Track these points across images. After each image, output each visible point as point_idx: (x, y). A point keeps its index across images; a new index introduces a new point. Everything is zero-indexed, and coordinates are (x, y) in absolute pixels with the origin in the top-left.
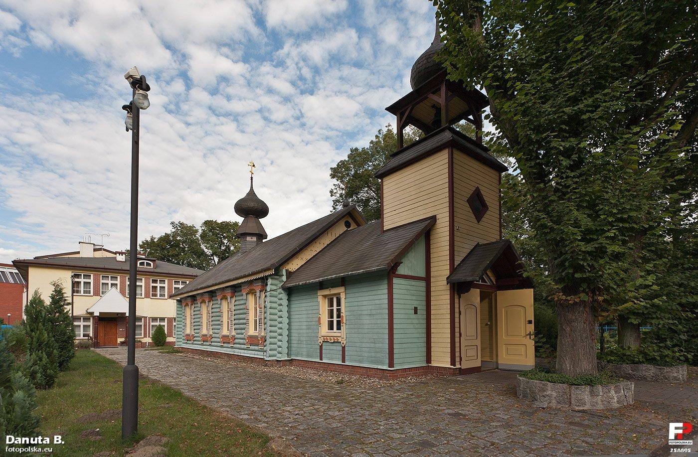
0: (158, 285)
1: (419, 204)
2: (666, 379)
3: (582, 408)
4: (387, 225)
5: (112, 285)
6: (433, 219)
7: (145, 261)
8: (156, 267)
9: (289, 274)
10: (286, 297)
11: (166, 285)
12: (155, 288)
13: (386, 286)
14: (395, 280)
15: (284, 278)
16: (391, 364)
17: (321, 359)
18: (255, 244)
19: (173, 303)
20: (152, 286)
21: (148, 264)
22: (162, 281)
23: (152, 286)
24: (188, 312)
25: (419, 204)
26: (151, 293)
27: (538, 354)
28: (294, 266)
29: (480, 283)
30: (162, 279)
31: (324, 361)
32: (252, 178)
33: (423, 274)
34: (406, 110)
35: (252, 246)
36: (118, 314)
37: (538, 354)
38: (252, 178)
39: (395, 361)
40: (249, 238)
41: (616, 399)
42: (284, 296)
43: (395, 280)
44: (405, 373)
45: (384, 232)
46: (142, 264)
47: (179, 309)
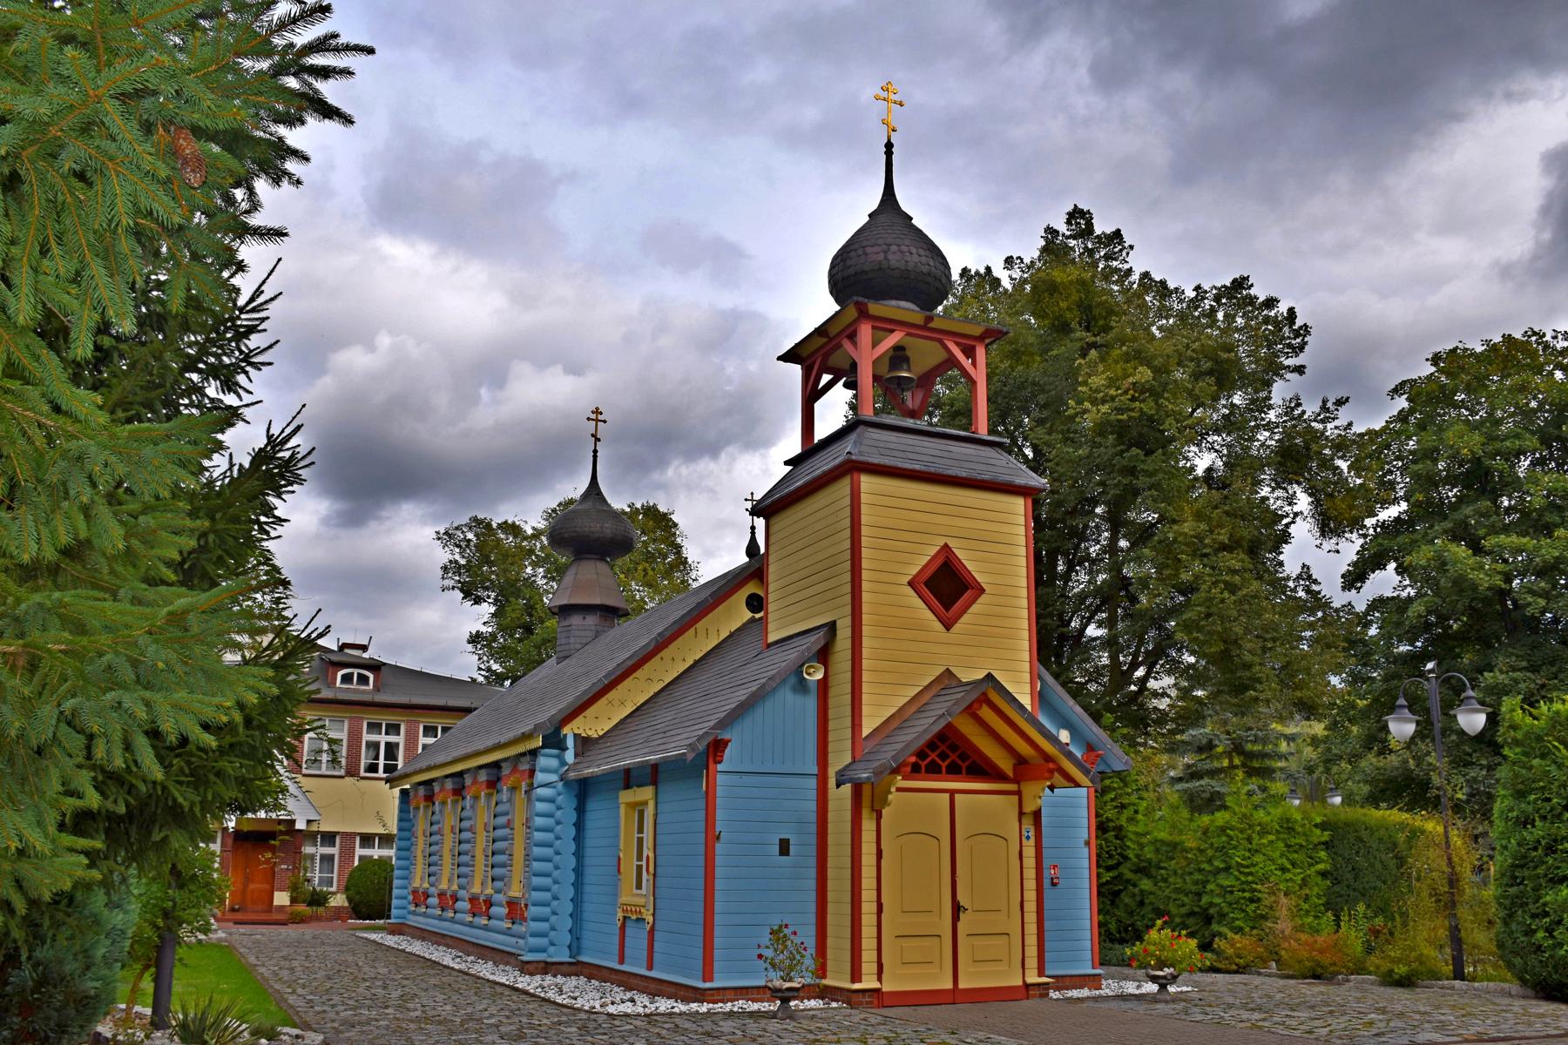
1: (811, 591)
3: (664, 1005)
5: (323, 857)
6: (832, 627)
7: (356, 671)
8: (377, 688)
9: (584, 743)
10: (574, 803)
11: (400, 739)
15: (570, 756)
17: (622, 961)
20: (398, 734)
21: (363, 680)
22: (393, 729)
23: (398, 734)
25: (811, 591)
27: (404, 815)
28: (593, 724)
30: (392, 718)
32: (889, 146)
34: (814, 362)
35: (584, 641)
37: (404, 815)
38: (889, 146)
45: (769, 646)
46: (347, 679)
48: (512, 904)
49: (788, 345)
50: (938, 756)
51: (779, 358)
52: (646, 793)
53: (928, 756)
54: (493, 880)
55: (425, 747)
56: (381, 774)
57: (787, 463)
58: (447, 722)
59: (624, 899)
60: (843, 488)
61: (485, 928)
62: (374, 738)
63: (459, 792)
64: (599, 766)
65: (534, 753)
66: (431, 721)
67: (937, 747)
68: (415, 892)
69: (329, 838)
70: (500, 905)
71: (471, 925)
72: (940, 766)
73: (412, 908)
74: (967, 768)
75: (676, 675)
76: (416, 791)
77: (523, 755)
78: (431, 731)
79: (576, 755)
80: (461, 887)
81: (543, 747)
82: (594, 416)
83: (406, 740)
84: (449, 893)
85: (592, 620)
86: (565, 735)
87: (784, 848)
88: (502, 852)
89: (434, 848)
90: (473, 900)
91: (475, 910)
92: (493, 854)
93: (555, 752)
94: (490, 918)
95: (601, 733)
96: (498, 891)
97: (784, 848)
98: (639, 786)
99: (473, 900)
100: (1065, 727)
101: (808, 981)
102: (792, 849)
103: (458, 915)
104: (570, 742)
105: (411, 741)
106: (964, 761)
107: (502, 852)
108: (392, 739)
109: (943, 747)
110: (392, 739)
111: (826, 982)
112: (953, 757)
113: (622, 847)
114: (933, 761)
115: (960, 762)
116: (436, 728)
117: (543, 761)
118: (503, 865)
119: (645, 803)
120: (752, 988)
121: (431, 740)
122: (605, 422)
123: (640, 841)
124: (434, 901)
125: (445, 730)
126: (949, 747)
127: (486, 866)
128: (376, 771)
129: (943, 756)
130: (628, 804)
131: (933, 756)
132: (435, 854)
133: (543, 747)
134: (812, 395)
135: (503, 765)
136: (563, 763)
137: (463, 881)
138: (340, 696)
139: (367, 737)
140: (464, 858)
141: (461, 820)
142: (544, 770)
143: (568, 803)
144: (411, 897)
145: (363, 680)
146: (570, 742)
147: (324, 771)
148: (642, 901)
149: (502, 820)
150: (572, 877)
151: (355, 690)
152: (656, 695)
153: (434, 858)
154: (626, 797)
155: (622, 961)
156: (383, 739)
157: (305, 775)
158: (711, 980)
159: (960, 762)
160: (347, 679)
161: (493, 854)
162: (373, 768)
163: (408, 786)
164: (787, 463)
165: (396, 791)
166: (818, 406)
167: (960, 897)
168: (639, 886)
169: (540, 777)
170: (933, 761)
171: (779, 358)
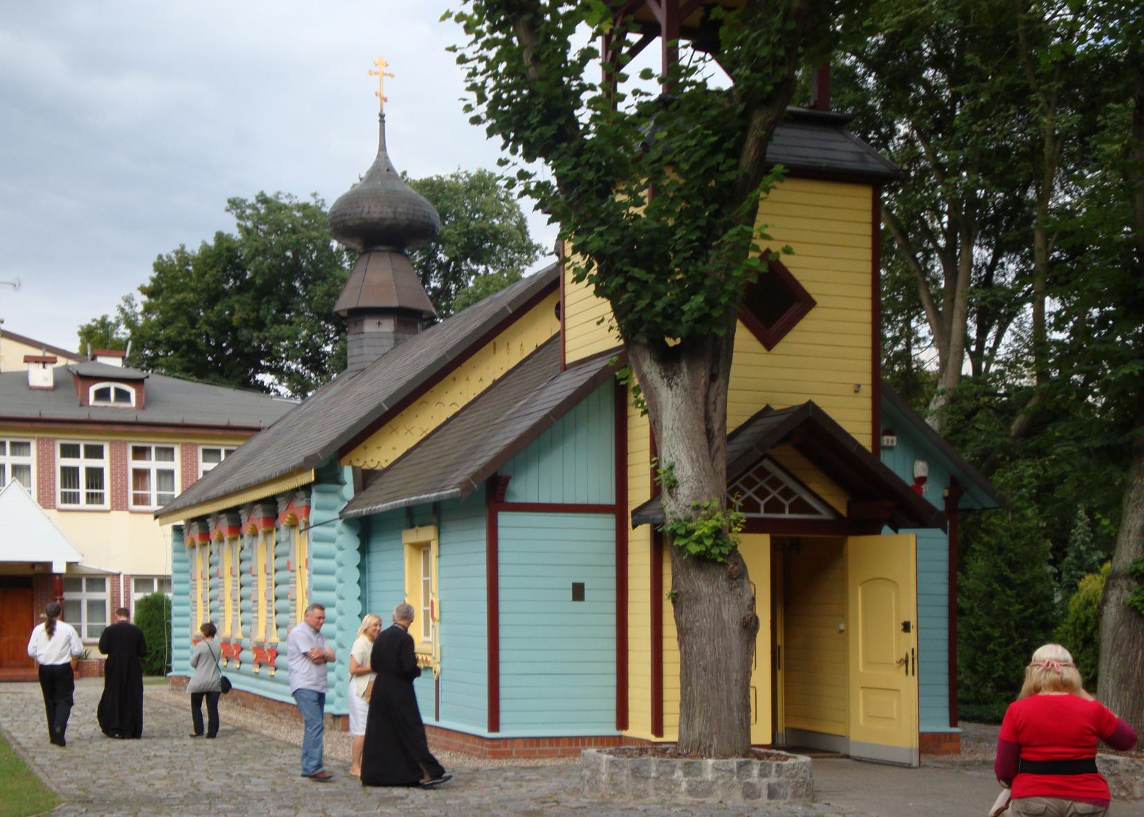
0: (153, 465)
2: (1124, 788)
4: (570, 358)
5: (16, 469)
7: (113, 386)
8: (144, 403)
9: (366, 479)
10: (356, 543)
11: (176, 465)
12: (141, 475)
13: (483, 534)
14: (504, 518)
15: (348, 491)
16: (494, 724)
17: (437, 719)
18: (389, 343)
19: (163, 533)
20: (172, 459)
21: (122, 396)
22: (166, 453)
24: (200, 564)
26: (131, 492)
29: (787, 515)
30: (165, 443)
31: (502, 733)
32: (382, 116)
33: (609, 498)
35: (382, 351)
36: (33, 565)
38: (382, 116)
39: (504, 717)
40: (370, 326)
41: (684, 786)
42: (348, 542)
43: (504, 518)
44: (538, 749)
46: (102, 395)
47: (180, 556)
50: (755, 493)
53: (768, 494)
54: (277, 627)
55: (205, 473)
58: (232, 444)
61: (272, 679)
62: (70, 462)
63: (236, 529)
64: (377, 503)
65: (307, 488)
66: (212, 444)
69: (96, 581)
71: (257, 675)
74: (766, 505)
75: (471, 397)
77: (296, 490)
78: (210, 454)
80: (245, 635)
82: (376, 69)
83: (112, 464)
85: (388, 326)
87: (578, 592)
88: (285, 597)
89: (214, 592)
91: (262, 660)
94: (276, 669)
95: (385, 465)
96: (284, 639)
97: (578, 592)
98: (421, 525)
100: (922, 458)
101: (785, 763)
103: (243, 666)
105: (189, 466)
106: (787, 499)
107: (285, 597)
108: (94, 463)
109: (762, 483)
110: (94, 463)
111: (624, 733)
112: (774, 494)
113: (407, 591)
115: (783, 500)
116: (78, 447)
118: (287, 611)
120: (544, 738)
121: (210, 466)
122: (392, 76)
123: (427, 584)
124: (248, 655)
125: (228, 452)
126: (768, 483)
127: (269, 612)
129: (762, 493)
137: (246, 628)
139: (62, 462)
140: (246, 603)
145: (122, 396)
149: (282, 562)
152: (448, 421)
153: (214, 604)
155: (437, 719)
156: (82, 463)
157: (133, 512)
160: (102, 395)
163: (181, 523)
165: (168, 529)
169: (315, 515)
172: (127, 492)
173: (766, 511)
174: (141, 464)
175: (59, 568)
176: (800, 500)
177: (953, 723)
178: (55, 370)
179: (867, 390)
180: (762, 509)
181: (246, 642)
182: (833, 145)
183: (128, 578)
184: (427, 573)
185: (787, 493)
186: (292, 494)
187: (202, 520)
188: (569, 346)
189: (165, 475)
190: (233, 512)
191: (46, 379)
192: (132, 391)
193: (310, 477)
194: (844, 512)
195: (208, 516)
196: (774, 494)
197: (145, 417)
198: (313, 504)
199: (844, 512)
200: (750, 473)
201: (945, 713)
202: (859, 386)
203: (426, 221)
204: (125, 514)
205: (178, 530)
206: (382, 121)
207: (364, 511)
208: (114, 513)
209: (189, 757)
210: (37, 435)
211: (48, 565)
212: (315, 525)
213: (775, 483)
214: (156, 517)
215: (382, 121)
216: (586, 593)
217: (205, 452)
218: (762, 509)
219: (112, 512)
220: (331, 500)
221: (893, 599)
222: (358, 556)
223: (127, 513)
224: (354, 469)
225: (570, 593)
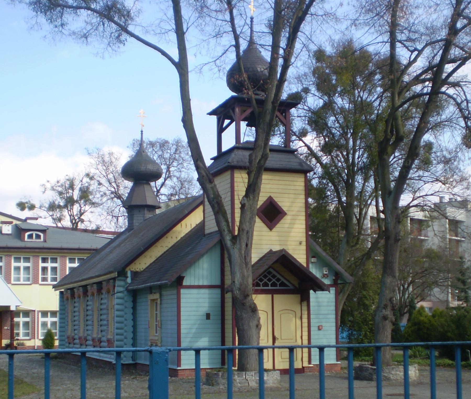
0: (49, 265)
7: (34, 233)
8: (45, 241)
9: (135, 274)
10: (131, 299)
15: (129, 280)
21: (38, 237)
22: (54, 260)
30: (54, 256)
32: (142, 132)
38: (142, 132)
43: (183, 291)
48: (108, 341)
49: (210, 110)
50: (276, 280)
51: (208, 114)
52: (157, 296)
53: (263, 280)
54: (101, 331)
56: (49, 282)
57: (212, 159)
59: (151, 338)
60: (227, 176)
65: (114, 279)
67: (267, 277)
68: (68, 337)
69: (27, 313)
70: (104, 342)
72: (277, 284)
73: (67, 345)
76: (67, 292)
79: (132, 279)
81: (118, 277)
84: (83, 338)
86: (127, 272)
90: (93, 340)
92: (101, 320)
93: (123, 278)
99: (93, 340)
102: (211, 317)
104: (129, 274)
108: (54, 265)
109: (270, 277)
112: (274, 280)
114: (266, 282)
115: (259, 282)
117: (117, 283)
119: (157, 299)
123: (156, 314)
124: (77, 341)
128: (47, 281)
129: (269, 280)
130: (151, 300)
131: (265, 280)
132: (104, 320)
133: (118, 277)
134: (221, 130)
135: (103, 283)
136: (127, 283)
138: (29, 245)
139: (41, 265)
141: (87, 306)
142: (118, 286)
143: (129, 299)
144: (67, 340)
145: (38, 237)
146: (129, 274)
147: (22, 282)
148: (156, 338)
150: (132, 329)
151: (35, 242)
154: (151, 297)
158: (180, 366)
159: (259, 282)
160: (30, 236)
161: (101, 320)
162: (44, 279)
163: (63, 290)
164: (212, 159)
165: (58, 292)
166: (223, 134)
167: (275, 334)
168: (156, 333)
169: (117, 289)
170: (274, 282)
171: (208, 114)
172: (38, 276)
173: (271, 286)
174: (45, 265)
175: (13, 308)
176: (283, 282)
177: (337, 361)
178: (12, 226)
179: (304, 243)
180: (270, 285)
181: (76, 337)
182: (292, 160)
183: (39, 311)
184: (156, 311)
185: (278, 280)
186: (108, 281)
187: (72, 289)
188: (206, 228)
189: (54, 269)
190: (85, 287)
191: (9, 230)
192: (42, 235)
193: (116, 274)
194: (297, 286)
195: (74, 288)
196: (274, 280)
197: (46, 245)
198: (116, 285)
199: (297, 286)
200: (266, 273)
201: (335, 357)
202: (302, 242)
203: (158, 171)
204: (37, 285)
205: (61, 293)
206: (142, 134)
207: (135, 287)
208: (33, 285)
209: (379, 295)
210: (5, 254)
211: (9, 307)
212: (117, 293)
213: (274, 276)
214: (53, 288)
215: (142, 134)
216: (211, 317)
217: (70, 259)
218: (270, 285)
219: (33, 285)
220: (122, 283)
221: (237, 336)
222: (132, 303)
223: (38, 285)
224: (131, 271)
225: (205, 317)
